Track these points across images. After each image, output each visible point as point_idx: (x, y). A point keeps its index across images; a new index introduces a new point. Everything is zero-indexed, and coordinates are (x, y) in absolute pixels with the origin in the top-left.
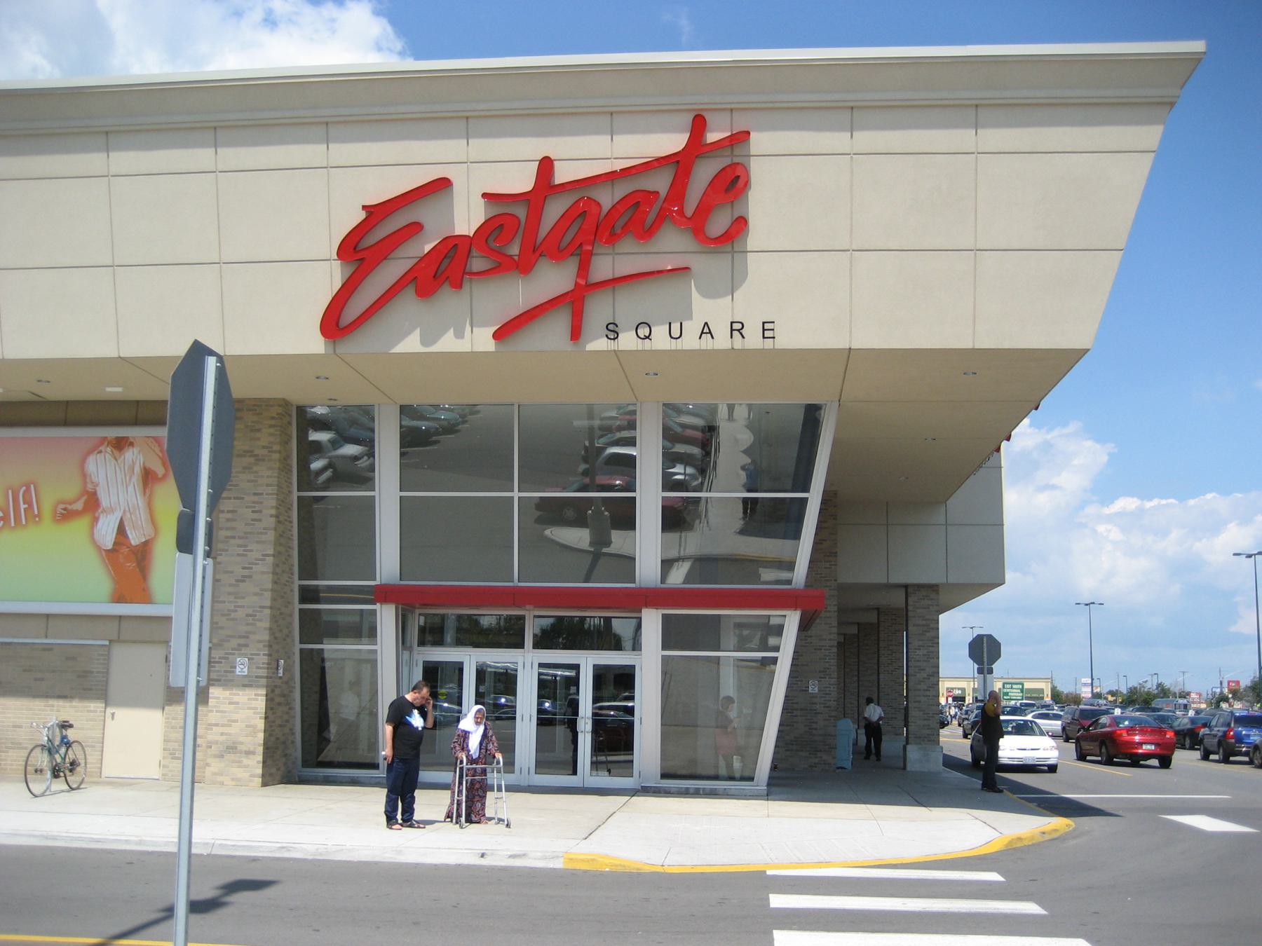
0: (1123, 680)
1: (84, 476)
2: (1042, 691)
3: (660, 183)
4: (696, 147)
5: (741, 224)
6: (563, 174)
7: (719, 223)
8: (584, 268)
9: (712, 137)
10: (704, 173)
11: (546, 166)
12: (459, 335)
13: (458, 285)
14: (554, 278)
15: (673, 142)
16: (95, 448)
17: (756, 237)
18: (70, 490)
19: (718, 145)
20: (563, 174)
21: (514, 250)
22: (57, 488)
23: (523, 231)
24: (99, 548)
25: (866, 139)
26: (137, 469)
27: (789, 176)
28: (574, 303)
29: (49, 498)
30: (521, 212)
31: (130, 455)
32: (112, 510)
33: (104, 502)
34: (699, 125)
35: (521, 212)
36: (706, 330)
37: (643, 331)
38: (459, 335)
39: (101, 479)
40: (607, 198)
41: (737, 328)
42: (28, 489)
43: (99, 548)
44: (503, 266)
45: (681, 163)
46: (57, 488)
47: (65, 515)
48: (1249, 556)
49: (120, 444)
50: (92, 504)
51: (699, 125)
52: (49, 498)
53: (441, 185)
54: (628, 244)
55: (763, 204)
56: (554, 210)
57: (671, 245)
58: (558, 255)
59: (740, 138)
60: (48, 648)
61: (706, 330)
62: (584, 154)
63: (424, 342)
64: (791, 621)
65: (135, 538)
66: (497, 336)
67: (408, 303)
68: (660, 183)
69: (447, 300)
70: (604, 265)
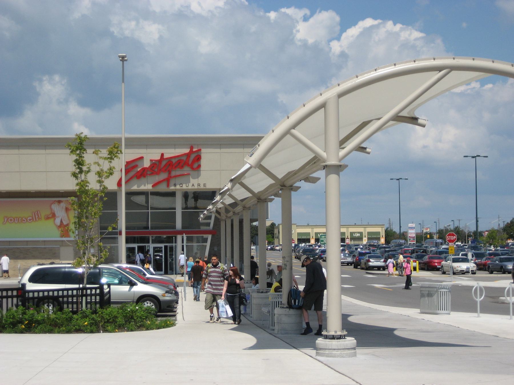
0: (452, 223)
1: (51, 209)
2: (379, 233)
3: (184, 158)
4: (191, 152)
5: (199, 166)
6: (165, 156)
7: (195, 165)
8: (170, 173)
9: (194, 150)
10: (193, 156)
11: (162, 155)
12: (145, 186)
13: (145, 177)
14: (163, 176)
15: (187, 151)
16: (54, 202)
17: (202, 168)
18: (48, 212)
19: (196, 151)
20: (165, 156)
21: (156, 170)
22: (45, 212)
23: (156, 167)
24: (56, 225)
25: (223, 150)
26: (64, 208)
27: (208, 156)
28: (168, 181)
29: (43, 215)
30: (157, 163)
31: (62, 204)
32: (58, 217)
33: (57, 215)
34: (192, 148)
35: (157, 163)
36: (193, 185)
37: (181, 185)
38: (145, 186)
39: (55, 210)
40: (174, 161)
41: (199, 185)
42: (38, 213)
43: (56, 225)
44: (153, 173)
45: (188, 155)
46: (45, 212)
47: (47, 218)
48: (473, 157)
49: (59, 202)
50: (54, 216)
51: (192, 148)
52: (43, 215)
53: (142, 158)
54: (178, 169)
55: (203, 162)
56: (164, 163)
57: (186, 170)
58: (165, 171)
59: (200, 150)
60: (45, 248)
61: (193, 185)
62: (170, 153)
63: (138, 187)
64: (210, 237)
65: (65, 223)
66: (153, 186)
67: (135, 180)
68: (184, 158)
69: (143, 179)
70: (173, 173)
